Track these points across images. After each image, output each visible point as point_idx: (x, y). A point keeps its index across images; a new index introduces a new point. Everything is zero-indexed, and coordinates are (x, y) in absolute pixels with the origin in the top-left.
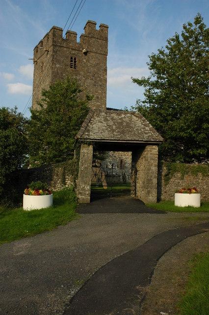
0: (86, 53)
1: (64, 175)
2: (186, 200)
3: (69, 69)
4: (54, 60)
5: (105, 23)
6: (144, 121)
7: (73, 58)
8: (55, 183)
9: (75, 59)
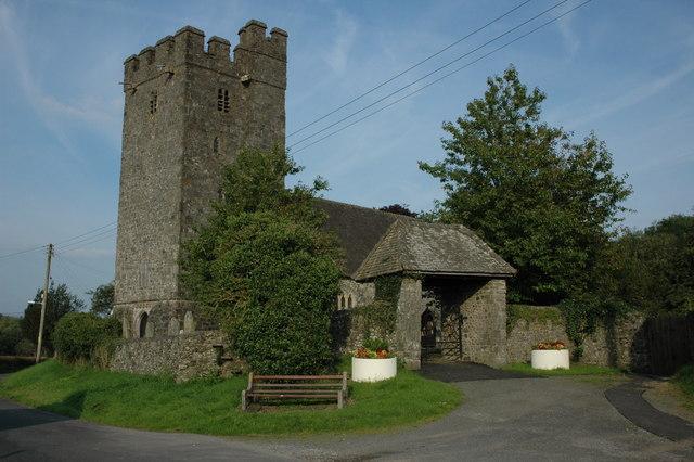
0: (246, 84)
1: (367, 326)
2: (552, 359)
3: (216, 112)
4: (189, 94)
5: (282, 27)
6: (477, 241)
7: (223, 91)
8: (353, 341)
9: (226, 93)
